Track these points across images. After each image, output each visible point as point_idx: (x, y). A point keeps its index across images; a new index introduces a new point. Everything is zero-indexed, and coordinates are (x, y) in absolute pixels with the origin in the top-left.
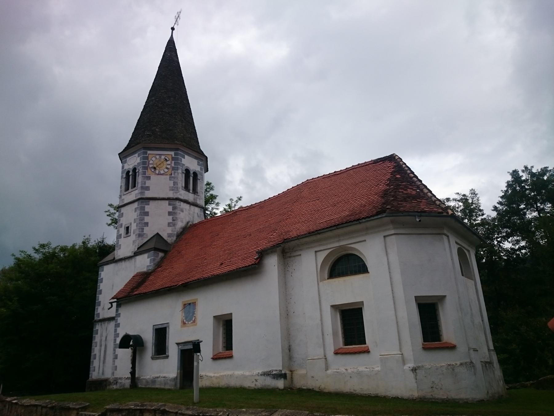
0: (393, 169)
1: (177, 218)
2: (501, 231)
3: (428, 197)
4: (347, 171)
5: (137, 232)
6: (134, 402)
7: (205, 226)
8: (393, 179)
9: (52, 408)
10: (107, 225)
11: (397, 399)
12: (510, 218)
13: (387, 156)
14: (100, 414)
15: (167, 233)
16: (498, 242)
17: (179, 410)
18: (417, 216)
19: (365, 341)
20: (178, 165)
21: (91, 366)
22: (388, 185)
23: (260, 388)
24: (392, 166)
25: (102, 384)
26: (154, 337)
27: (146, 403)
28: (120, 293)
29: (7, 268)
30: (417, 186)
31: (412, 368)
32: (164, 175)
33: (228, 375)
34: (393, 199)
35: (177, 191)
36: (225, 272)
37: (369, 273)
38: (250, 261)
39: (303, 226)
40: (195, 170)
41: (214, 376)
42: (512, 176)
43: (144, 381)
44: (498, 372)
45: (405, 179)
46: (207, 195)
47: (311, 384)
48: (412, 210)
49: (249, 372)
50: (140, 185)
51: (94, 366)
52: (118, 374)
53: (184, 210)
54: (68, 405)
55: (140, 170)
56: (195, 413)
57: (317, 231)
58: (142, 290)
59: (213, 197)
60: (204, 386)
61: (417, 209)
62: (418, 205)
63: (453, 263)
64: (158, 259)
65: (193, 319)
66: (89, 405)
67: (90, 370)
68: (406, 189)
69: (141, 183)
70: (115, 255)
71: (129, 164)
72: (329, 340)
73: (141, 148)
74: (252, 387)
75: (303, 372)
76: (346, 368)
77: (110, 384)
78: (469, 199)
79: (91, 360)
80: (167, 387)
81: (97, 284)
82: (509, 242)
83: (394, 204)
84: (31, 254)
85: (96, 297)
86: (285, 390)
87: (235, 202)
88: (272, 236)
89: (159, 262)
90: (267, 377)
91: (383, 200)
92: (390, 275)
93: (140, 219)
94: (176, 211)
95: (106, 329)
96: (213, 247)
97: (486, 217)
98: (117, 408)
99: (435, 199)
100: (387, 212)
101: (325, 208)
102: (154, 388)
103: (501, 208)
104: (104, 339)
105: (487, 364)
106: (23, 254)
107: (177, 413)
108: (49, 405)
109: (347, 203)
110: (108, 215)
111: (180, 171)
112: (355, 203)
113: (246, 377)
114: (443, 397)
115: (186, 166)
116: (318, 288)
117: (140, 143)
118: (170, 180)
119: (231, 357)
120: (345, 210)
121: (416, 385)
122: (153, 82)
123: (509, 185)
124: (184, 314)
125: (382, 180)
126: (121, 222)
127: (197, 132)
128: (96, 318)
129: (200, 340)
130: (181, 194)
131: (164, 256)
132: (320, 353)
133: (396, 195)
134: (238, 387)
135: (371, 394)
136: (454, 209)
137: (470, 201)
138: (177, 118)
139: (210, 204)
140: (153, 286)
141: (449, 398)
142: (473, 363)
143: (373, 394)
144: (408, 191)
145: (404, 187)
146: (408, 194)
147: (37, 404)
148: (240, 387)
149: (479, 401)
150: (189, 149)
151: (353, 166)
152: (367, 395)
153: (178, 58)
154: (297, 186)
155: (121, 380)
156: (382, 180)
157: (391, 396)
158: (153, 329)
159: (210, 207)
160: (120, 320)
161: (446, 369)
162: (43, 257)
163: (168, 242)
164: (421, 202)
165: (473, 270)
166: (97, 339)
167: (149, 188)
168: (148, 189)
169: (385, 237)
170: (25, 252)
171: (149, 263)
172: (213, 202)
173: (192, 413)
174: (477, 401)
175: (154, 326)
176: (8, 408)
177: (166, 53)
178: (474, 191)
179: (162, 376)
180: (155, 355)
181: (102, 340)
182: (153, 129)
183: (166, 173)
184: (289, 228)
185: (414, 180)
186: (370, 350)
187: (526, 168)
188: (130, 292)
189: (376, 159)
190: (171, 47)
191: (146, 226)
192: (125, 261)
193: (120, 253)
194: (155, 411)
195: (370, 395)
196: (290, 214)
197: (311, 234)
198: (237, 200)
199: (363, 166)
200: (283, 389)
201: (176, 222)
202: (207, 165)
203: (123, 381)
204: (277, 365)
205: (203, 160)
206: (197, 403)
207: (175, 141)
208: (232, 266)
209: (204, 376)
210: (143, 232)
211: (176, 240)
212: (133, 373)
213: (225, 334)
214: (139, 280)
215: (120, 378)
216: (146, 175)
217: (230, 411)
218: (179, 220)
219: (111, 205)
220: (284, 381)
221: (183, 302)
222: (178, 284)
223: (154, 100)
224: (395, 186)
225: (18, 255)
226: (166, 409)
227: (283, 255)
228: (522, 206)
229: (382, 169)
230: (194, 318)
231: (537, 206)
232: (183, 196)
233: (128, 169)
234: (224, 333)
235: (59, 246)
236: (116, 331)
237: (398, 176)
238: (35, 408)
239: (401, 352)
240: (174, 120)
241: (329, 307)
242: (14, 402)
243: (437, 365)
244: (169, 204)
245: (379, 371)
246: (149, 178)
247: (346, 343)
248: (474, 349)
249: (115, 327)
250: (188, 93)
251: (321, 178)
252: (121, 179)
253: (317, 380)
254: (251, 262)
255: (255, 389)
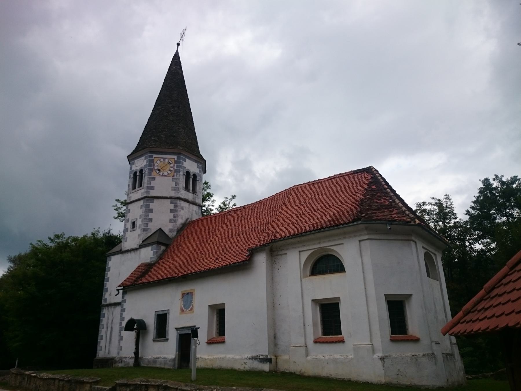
0: (369, 180)
1: (177, 215)
2: (472, 234)
3: (399, 207)
4: (330, 179)
5: (142, 227)
6: (140, 379)
7: (202, 223)
8: (369, 190)
9: (69, 381)
10: (114, 218)
11: (366, 384)
12: (481, 221)
13: (365, 168)
14: (111, 387)
15: (168, 228)
16: (470, 243)
17: (179, 387)
18: (388, 224)
19: (341, 334)
20: (180, 168)
21: (98, 346)
22: (364, 195)
23: (248, 370)
24: (369, 178)
25: (108, 362)
26: (156, 322)
27: (150, 380)
28: (126, 281)
29: (22, 254)
30: (390, 196)
31: (380, 357)
32: (167, 176)
33: (221, 357)
34: (368, 208)
35: (178, 191)
36: (220, 267)
37: (345, 272)
38: (241, 258)
39: (289, 228)
40: (195, 172)
41: (208, 358)
42: (484, 184)
43: (146, 361)
44: (459, 363)
45: (380, 190)
46: (204, 193)
47: (292, 368)
48: (383, 218)
49: (239, 356)
50: (145, 185)
51: (101, 345)
52: (123, 354)
53: (184, 209)
54: (83, 379)
55: (146, 171)
56: (193, 389)
57: (301, 233)
58: (146, 279)
59: (209, 195)
60: (199, 367)
61: (388, 218)
62: (389, 214)
63: (419, 266)
64: (160, 252)
65: (191, 307)
66: (100, 380)
67: (97, 350)
68: (380, 200)
69: (147, 183)
70: (122, 246)
71: (137, 165)
72: (310, 330)
73: (147, 152)
74: (241, 369)
75: (286, 357)
76: (323, 355)
77: (116, 362)
78: (444, 204)
79: (98, 340)
80: (167, 367)
81: (105, 272)
82: (480, 244)
83: (368, 212)
84: (46, 244)
85: (103, 283)
86: (270, 373)
87: (229, 200)
88: (262, 236)
89: (161, 254)
90: (254, 361)
91: (359, 208)
92: (364, 275)
93: (145, 216)
94: (177, 209)
95: (113, 313)
96: (209, 243)
97: (458, 221)
98: (126, 383)
99: (404, 210)
100: (362, 220)
101: (309, 213)
102: (155, 367)
103: (473, 212)
104: (110, 321)
105: (449, 356)
106: (39, 243)
107: (177, 389)
108: (66, 378)
109: (328, 209)
110: (115, 209)
111: (181, 173)
112: (335, 210)
113: (236, 360)
114: (407, 384)
115: (187, 168)
116: (301, 284)
117: (147, 147)
118: (172, 181)
119: (223, 342)
120: (326, 216)
121: (383, 372)
122: (159, 92)
123: (481, 192)
124: (182, 302)
125: (359, 190)
126: (128, 218)
127: (197, 138)
128: (103, 303)
129: (197, 327)
130: (182, 194)
131: (165, 249)
132: (302, 341)
133: (371, 205)
134: (229, 369)
135: (344, 378)
136: (430, 212)
137: (444, 205)
138: (181, 126)
139: (206, 201)
140: (155, 276)
141: (412, 384)
142: (434, 354)
143: (347, 379)
144: (381, 201)
145: (378, 197)
146: (381, 204)
147: (55, 377)
148: (230, 369)
149: (438, 388)
150: (190, 153)
151: (335, 175)
152: (341, 380)
153: (182, 71)
154: (285, 190)
155: (125, 359)
156: (359, 190)
157: (362, 381)
158: (155, 315)
159: (206, 204)
160: (125, 306)
161: (410, 359)
162: (58, 247)
163: (170, 236)
164: (392, 211)
165: (439, 272)
166: (104, 321)
167: (154, 188)
168: (153, 189)
169: (360, 241)
170: (41, 241)
171: (152, 255)
172: (209, 200)
173: (190, 389)
174: (437, 388)
175: (156, 312)
176: (27, 380)
177: (172, 66)
178: (448, 196)
179: (162, 357)
180: (156, 338)
181: (108, 322)
182: (158, 135)
183: (169, 174)
184: (277, 230)
185: (387, 191)
186: (345, 340)
187: (497, 176)
188: (135, 281)
189: (355, 170)
190: (176, 61)
191: (151, 221)
192: (131, 252)
193: (126, 245)
194: (158, 386)
195: (344, 379)
196: (278, 216)
197: (296, 236)
198: (231, 199)
199: (344, 176)
200: (268, 372)
201: (176, 218)
202: (206, 169)
203: (127, 360)
204: (264, 351)
205: (202, 163)
206: (195, 381)
207: (178, 146)
208: (226, 261)
209: (199, 358)
210: (148, 227)
211: (176, 235)
212: (136, 353)
213: (219, 325)
214: (143, 270)
215: (125, 357)
216: (151, 176)
217: (222, 388)
218: (180, 217)
219: (118, 200)
220: (270, 365)
221: (182, 291)
222: (178, 276)
223: (160, 109)
224: (371, 196)
225: (35, 243)
226: (168, 385)
227: (271, 254)
228: (492, 212)
229: (360, 180)
230: (191, 306)
231: (505, 212)
232: (184, 196)
233: (135, 170)
234: (218, 329)
235: (71, 236)
236: (121, 315)
237: (374, 187)
238: (53, 381)
239: (371, 342)
240: (177, 128)
241: (310, 301)
242: (33, 375)
243: (403, 355)
244: (171, 203)
245: (352, 359)
246: (154, 179)
247: (325, 333)
248: (435, 342)
249: (121, 312)
250: (190, 103)
251: (307, 184)
252: (129, 179)
253: (298, 365)
254: (243, 258)
255: (244, 371)
